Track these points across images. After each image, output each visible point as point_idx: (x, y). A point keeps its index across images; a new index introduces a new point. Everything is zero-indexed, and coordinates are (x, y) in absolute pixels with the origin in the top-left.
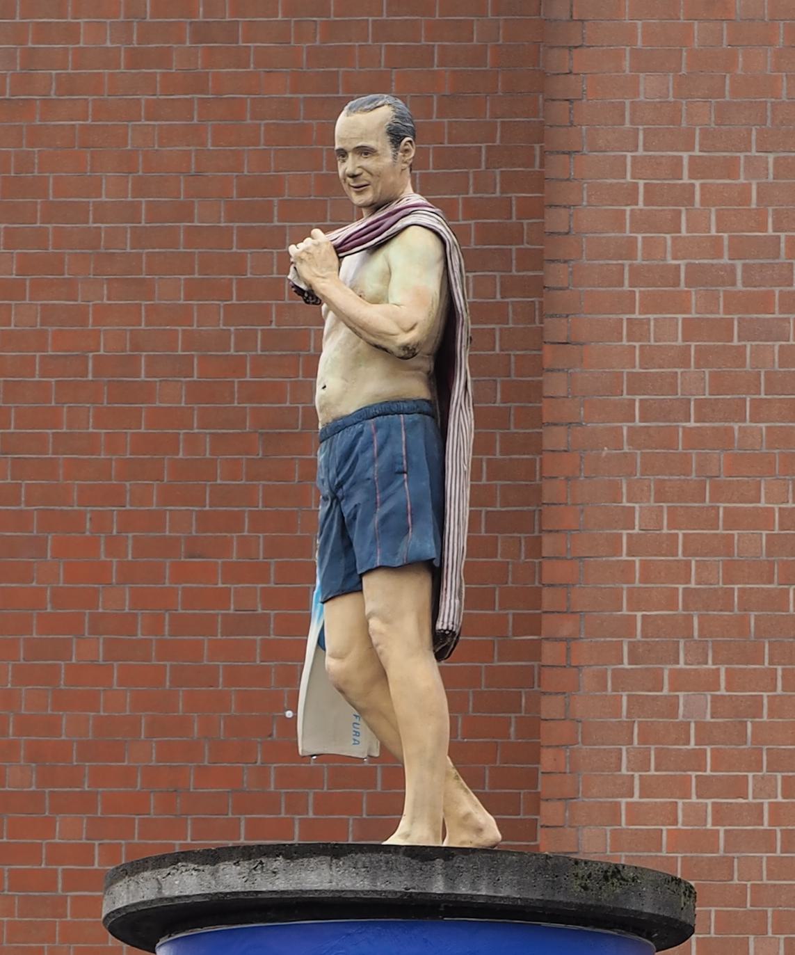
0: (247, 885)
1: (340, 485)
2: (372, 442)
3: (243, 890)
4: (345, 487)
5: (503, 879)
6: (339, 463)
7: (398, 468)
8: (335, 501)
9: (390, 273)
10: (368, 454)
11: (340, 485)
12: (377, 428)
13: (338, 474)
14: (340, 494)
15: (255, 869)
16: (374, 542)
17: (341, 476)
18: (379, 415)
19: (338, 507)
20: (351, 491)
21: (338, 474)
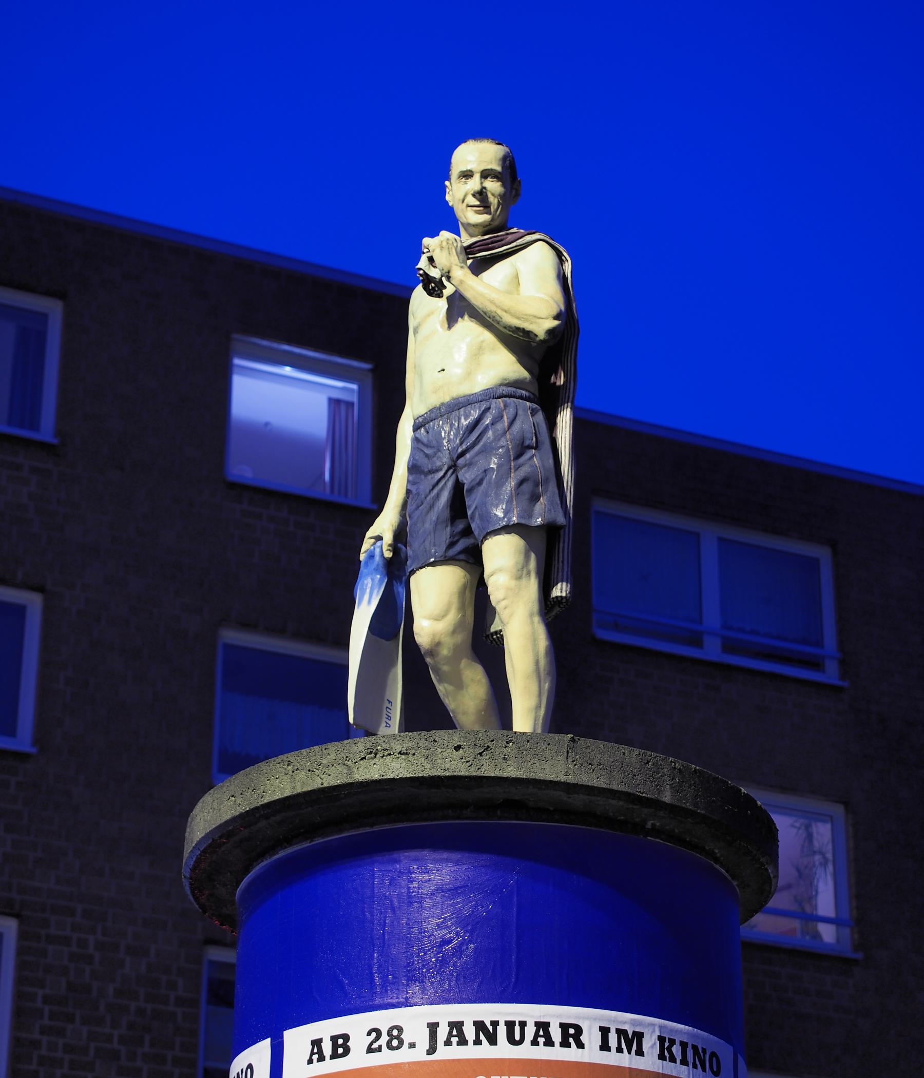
0: (472, 769)
1: (462, 454)
2: (502, 417)
3: (467, 774)
4: (468, 456)
5: (847, 931)
6: (464, 434)
7: (527, 443)
8: (451, 470)
9: (517, 277)
10: (499, 426)
11: (462, 454)
12: (506, 406)
13: (461, 444)
14: (461, 461)
15: (481, 754)
16: (509, 502)
17: (464, 447)
18: (505, 396)
19: (454, 476)
20: (476, 459)
21: (461, 444)
